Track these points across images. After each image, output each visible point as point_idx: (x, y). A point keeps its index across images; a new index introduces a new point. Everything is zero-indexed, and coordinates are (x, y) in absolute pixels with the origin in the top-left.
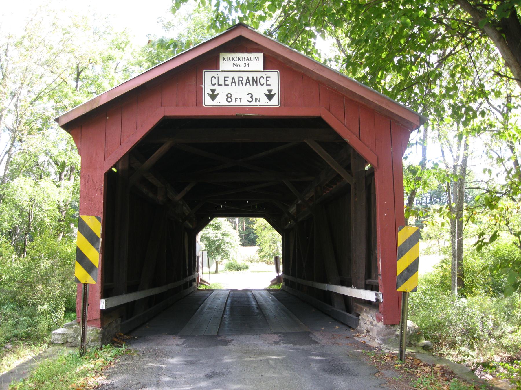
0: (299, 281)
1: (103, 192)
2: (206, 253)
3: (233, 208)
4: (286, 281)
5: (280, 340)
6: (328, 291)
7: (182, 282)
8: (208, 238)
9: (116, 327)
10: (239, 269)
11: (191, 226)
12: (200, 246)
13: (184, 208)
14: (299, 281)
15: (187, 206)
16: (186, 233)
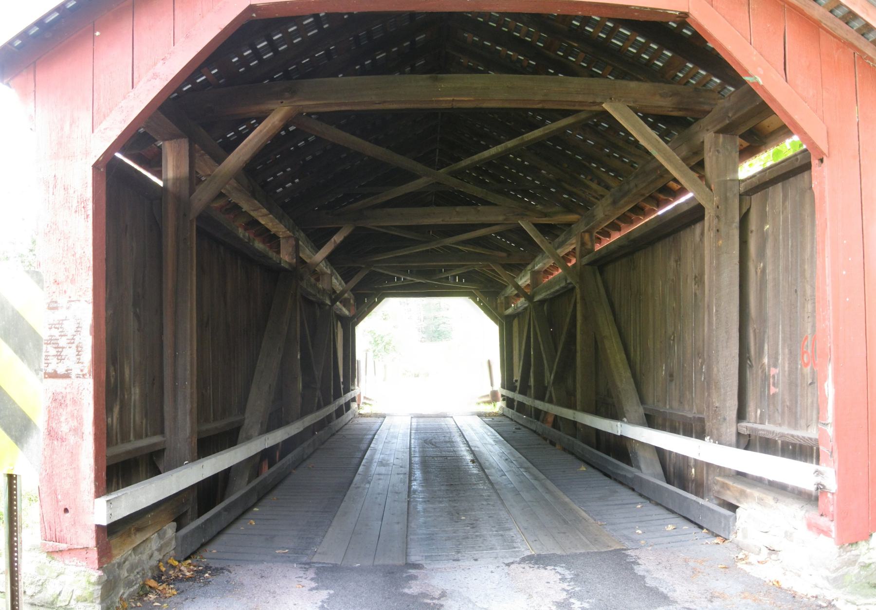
1: (90, 213)
4: (510, 403)
5: (571, 594)
6: (621, 436)
7: (332, 408)
9: (159, 550)
11: (347, 312)
13: (334, 281)
15: (340, 278)
16: (339, 324)
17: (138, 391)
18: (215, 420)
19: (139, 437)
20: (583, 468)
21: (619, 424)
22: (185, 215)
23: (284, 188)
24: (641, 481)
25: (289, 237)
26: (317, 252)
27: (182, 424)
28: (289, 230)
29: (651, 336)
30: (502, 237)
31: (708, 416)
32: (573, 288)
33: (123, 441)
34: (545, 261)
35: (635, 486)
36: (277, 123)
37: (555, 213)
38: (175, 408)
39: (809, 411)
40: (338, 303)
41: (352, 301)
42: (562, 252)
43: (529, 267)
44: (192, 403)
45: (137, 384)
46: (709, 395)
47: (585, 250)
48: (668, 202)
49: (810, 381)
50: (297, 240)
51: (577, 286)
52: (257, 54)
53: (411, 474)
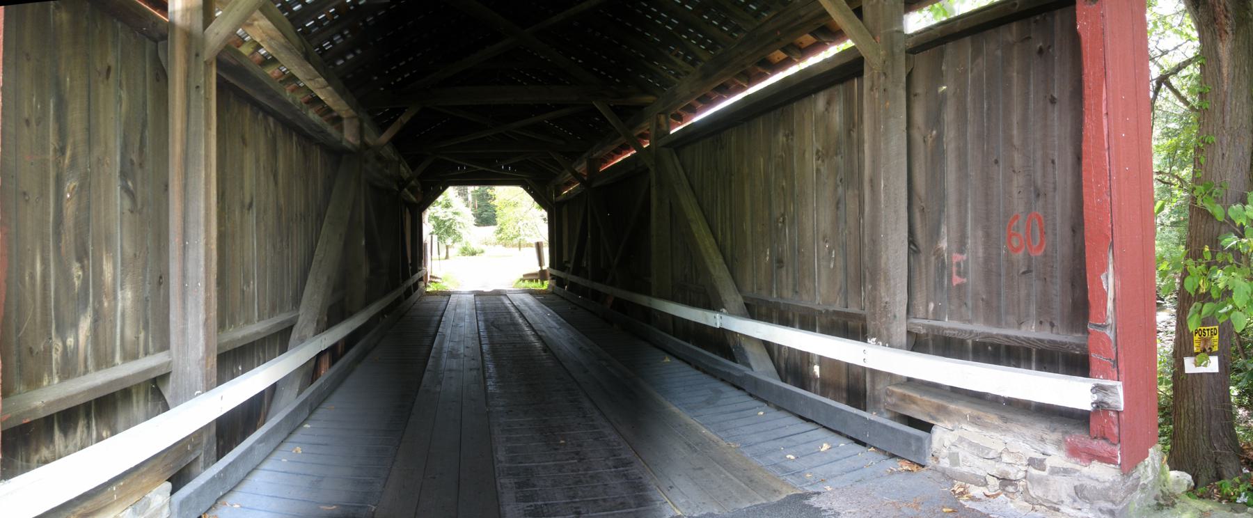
0: (598, 286)
2: (435, 237)
3: (480, 168)
4: (559, 282)
8: (436, 218)
10: (474, 254)
12: (427, 228)
14: (598, 286)
17: (129, 294)
18: (261, 318)
19: (130, 356)
20: (667, 360)
21: (718, 315)
22: (197, 55)
23: (345, 60)
24: (756, 382)
27: (193, 336)
29: (748, 217)
31: (874, 314)
33: (98, 367)
35: (739, 384)
38: (184, 317)
39: (1022, 306)
43: (586, 155)
44: (207, 310)
45: (128, 286)
46: (875, 288)
48: (762, 77)
49: (1023, 270)
53: (483, 368)
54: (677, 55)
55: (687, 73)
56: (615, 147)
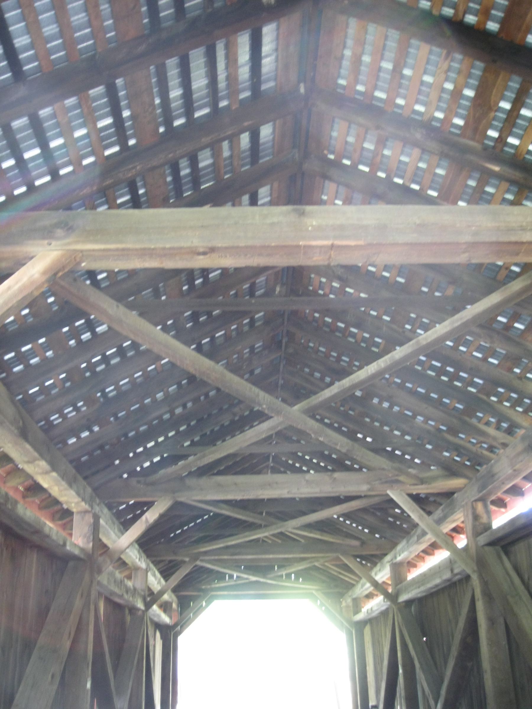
15: (157, 573)
16: (158, 634)
23: (79, 438)
25: (86, 512)
26: (123, 534)
28: (83, 500)
30: (353, 520)
32: (468, 578)
34: (411, 549)
36: (37, 276)
37: (434, 479)
40: (155, 607)
41: (174, 606)
42: (447, 528)
43: (388, 558)
47: (480, 528)
50: (97, 518)
51: (475, 577)
52: (105, 359)
54: (488, 423)
55: (505, 445)
56: (423, 546)
